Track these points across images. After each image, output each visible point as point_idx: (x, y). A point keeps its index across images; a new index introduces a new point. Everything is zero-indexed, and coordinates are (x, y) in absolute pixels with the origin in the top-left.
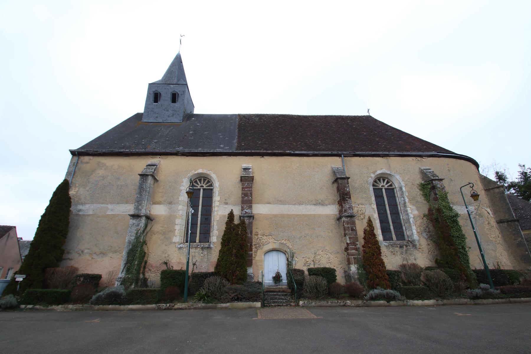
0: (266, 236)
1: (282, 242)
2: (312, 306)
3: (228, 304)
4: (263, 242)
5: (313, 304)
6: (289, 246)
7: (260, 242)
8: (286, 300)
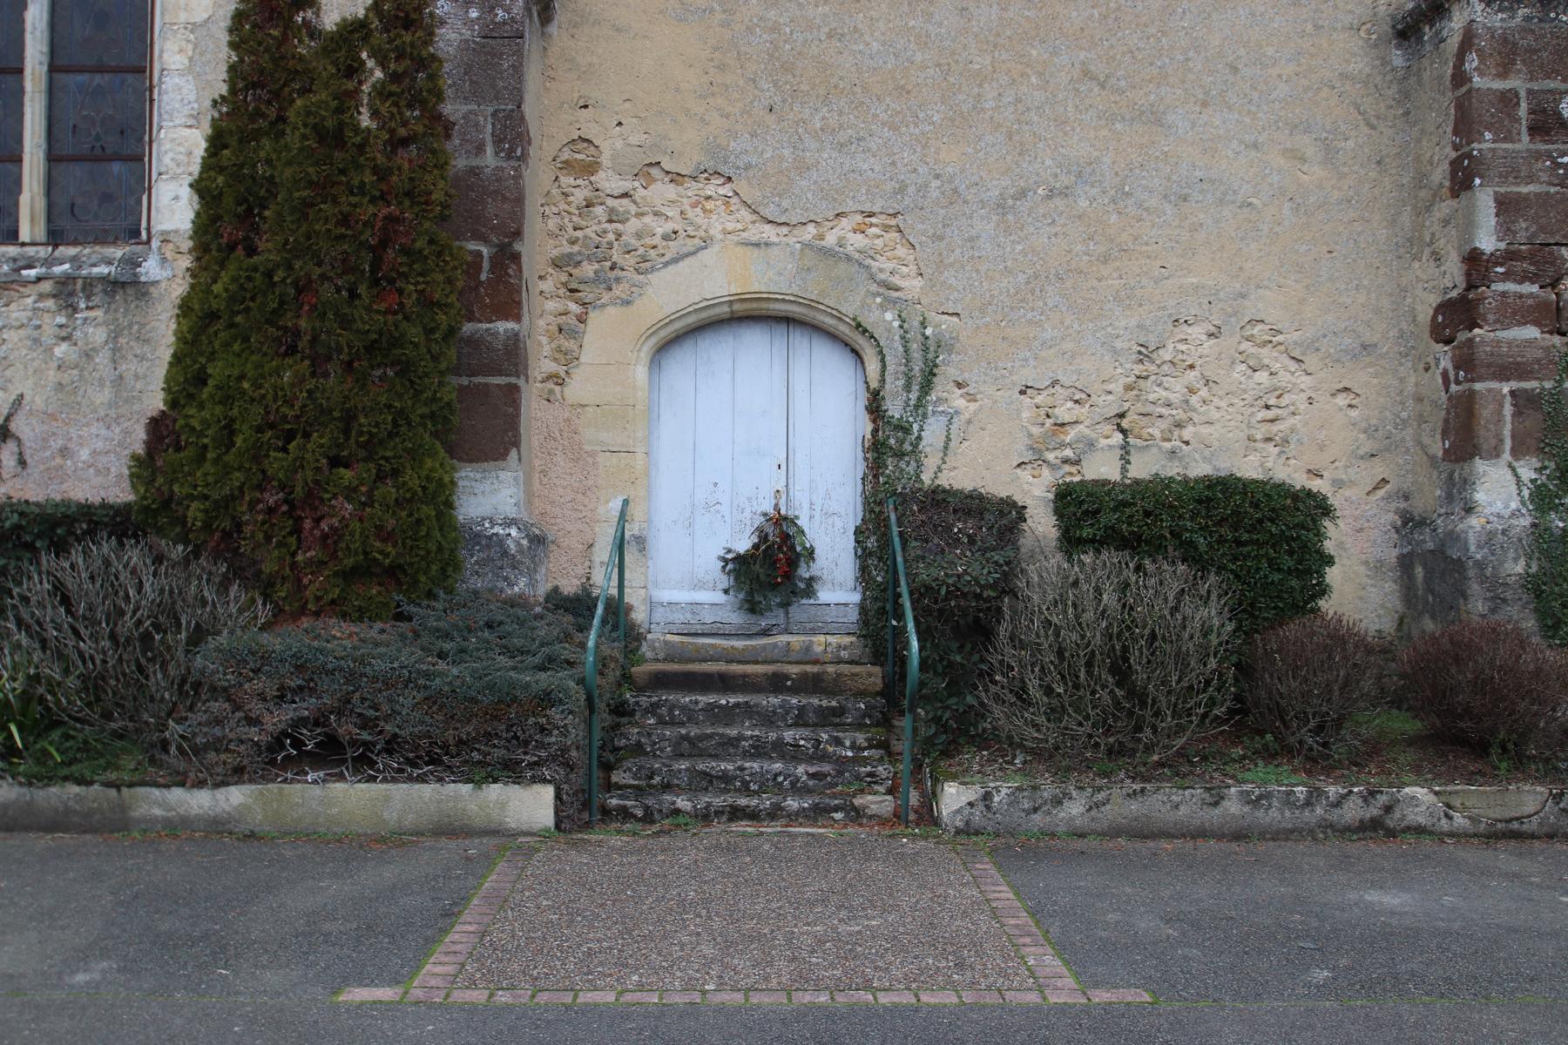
0: (676, 178)
1: (831, 240)
2: (1062, 829)
3: (235, 797)
4: (639, 235)
5: (1075, 809)
6: (896, 280)
7: (619, 235)
8: (824, 757)
